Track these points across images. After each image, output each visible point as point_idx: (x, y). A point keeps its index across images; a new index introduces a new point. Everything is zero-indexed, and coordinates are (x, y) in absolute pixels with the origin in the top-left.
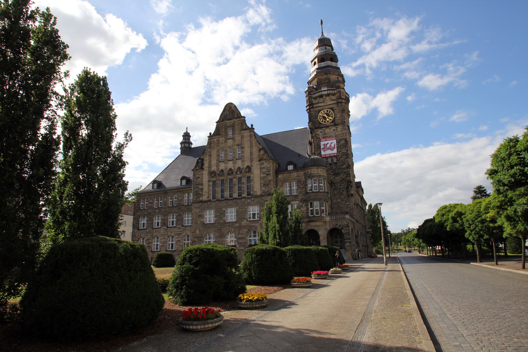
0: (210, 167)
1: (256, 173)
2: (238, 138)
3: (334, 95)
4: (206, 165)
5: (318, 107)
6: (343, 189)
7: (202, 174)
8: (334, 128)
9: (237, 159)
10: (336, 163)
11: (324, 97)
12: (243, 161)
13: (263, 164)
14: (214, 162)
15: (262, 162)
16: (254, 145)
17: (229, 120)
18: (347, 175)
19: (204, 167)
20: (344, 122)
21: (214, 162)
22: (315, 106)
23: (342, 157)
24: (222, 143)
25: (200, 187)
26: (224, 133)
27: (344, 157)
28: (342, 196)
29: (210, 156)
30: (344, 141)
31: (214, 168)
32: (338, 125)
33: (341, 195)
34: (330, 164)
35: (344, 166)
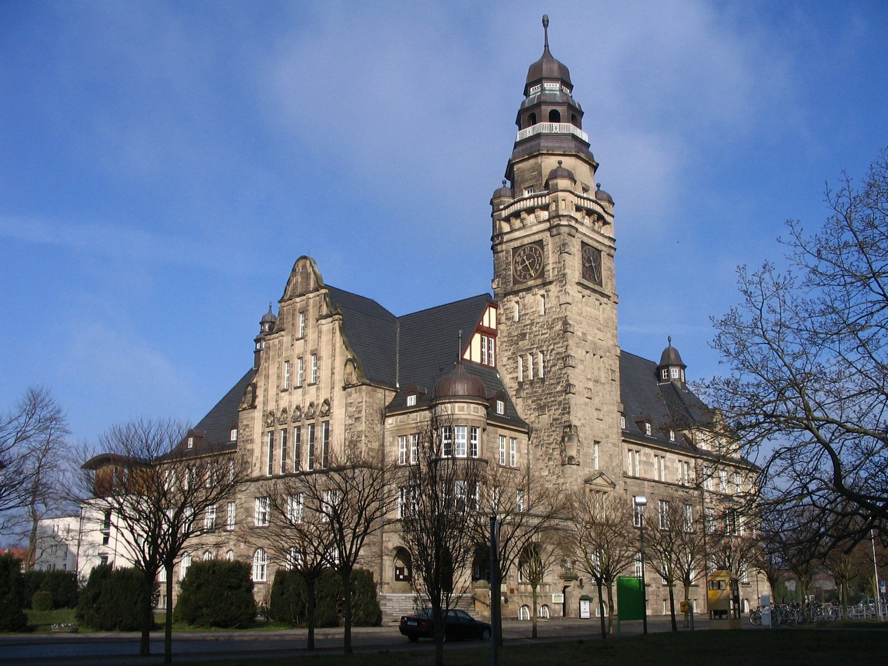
0: (265, 403)
1: (339, 417)
2: (312, 335)
3: (545, 207)
4: (259, 401)
5: (511, 240)
6: (553, 446)
7: (253, 419)
8: (542, 292)
9: (309, 385)
10: (543, 380)
11: (524, 215)
12: (318, 389)
13: (350, 395)
14: (272, 392)
15: (348, 390)
16: (338, 350)
17: (300, 296)
18: (564, 409)
19: (256, 403)
20: (564, 275)
21: (272, 392)
22: (506, 238)
23: (555, 365)
24: (286, 350)
25: (823, 267)
26: (290, 327)
27: (560, 364)
28: (551, 463)
29: (267, 377)
30: (560, 323)
31: (271, 406)
32: (551, 283)
33: (549, 459)
34: (532, 383)
35: (559, 388)
